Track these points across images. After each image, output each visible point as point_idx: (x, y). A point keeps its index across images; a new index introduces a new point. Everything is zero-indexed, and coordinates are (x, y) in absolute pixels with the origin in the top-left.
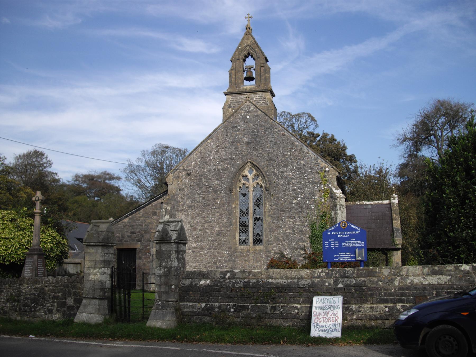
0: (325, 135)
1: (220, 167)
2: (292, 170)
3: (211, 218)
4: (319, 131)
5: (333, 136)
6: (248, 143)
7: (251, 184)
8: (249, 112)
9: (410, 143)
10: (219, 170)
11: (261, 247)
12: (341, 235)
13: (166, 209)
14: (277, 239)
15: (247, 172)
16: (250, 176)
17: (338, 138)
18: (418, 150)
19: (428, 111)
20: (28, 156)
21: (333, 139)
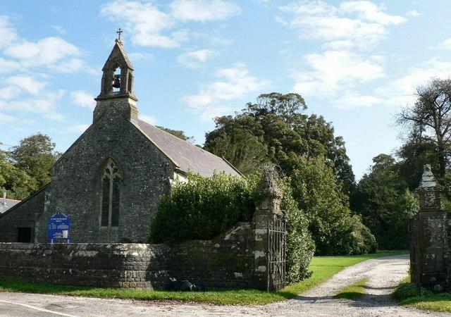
0: (313, 117)
1: (89, 161)
2: (141, 164)
3: (80, 203)
4: (308, 113)
5: (321, 117)
6: (110, 141)
7: (111, 177)
8: (112, 115)
9: (413, 122)
10: (88, 164)
11: (116, 228)
12: (58, 220)
13: (47, 196)
14: (128, 222)
15: (109, 167)
16: (111, 169)
17: (327, 120)
18: (422, 130)
19: (239, 116)
20: (32, 139)
21: (321, 120)
